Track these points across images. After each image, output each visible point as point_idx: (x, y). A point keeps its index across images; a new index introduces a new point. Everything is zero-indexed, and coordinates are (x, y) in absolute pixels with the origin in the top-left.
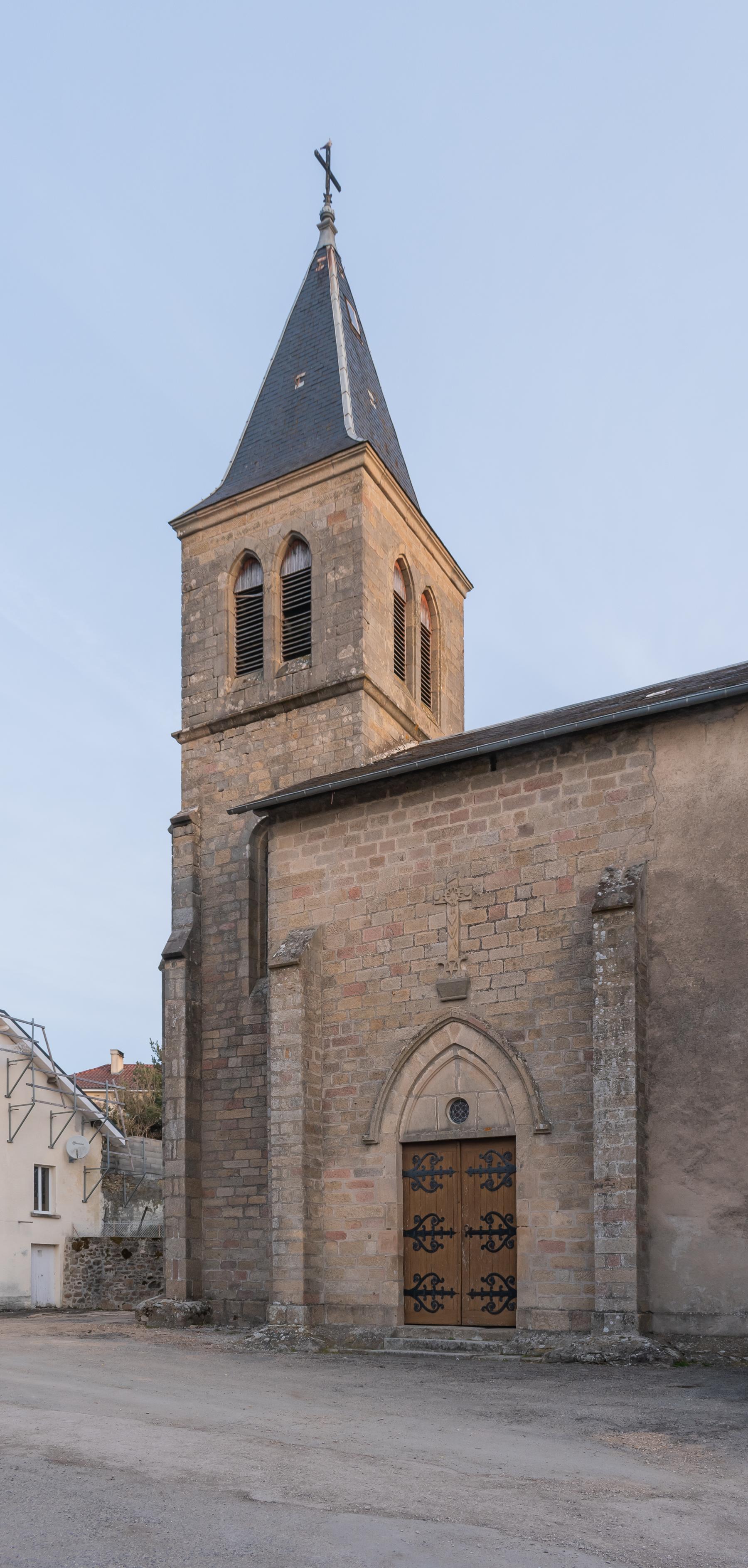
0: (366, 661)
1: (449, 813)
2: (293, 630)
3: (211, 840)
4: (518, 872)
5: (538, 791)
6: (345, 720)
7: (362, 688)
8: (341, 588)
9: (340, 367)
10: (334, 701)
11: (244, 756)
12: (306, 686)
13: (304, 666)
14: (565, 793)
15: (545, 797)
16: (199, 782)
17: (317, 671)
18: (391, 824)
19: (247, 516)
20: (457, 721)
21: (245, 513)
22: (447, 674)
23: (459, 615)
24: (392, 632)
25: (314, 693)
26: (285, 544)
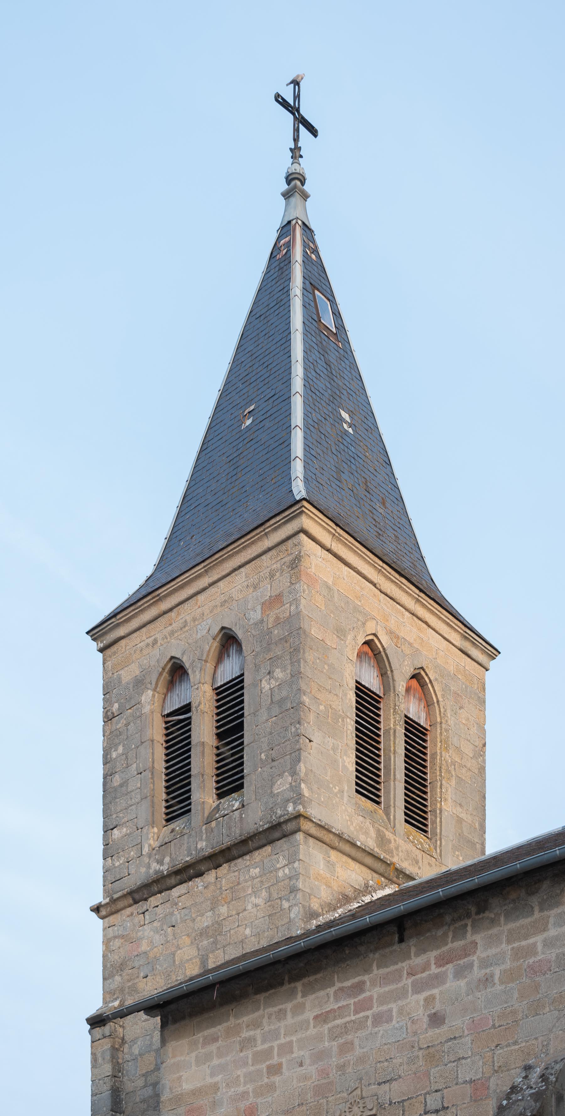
0: (306, 793)
1: (352, 1001)
2: (233, 755)
3: (134, 1041)
4: (427, 1074)
5: (450, 966)
6: (280, 874)
7: (299, 830)
8: (276, 698)
9: (293, 392)
10: (268, 849)
11: (170, 930)
12: (238, 831)
13: (237, 805)
14: (480, 967)
15: (459, 974)
16: (121, 967)
17: (250, 812)
18: (290, 1020)
19: (173, 614)
20: (472, 844)
21: (171, 610)
22: (453, 782)
24: (353, 745)
25: (244, 842)
26: (216, 644)
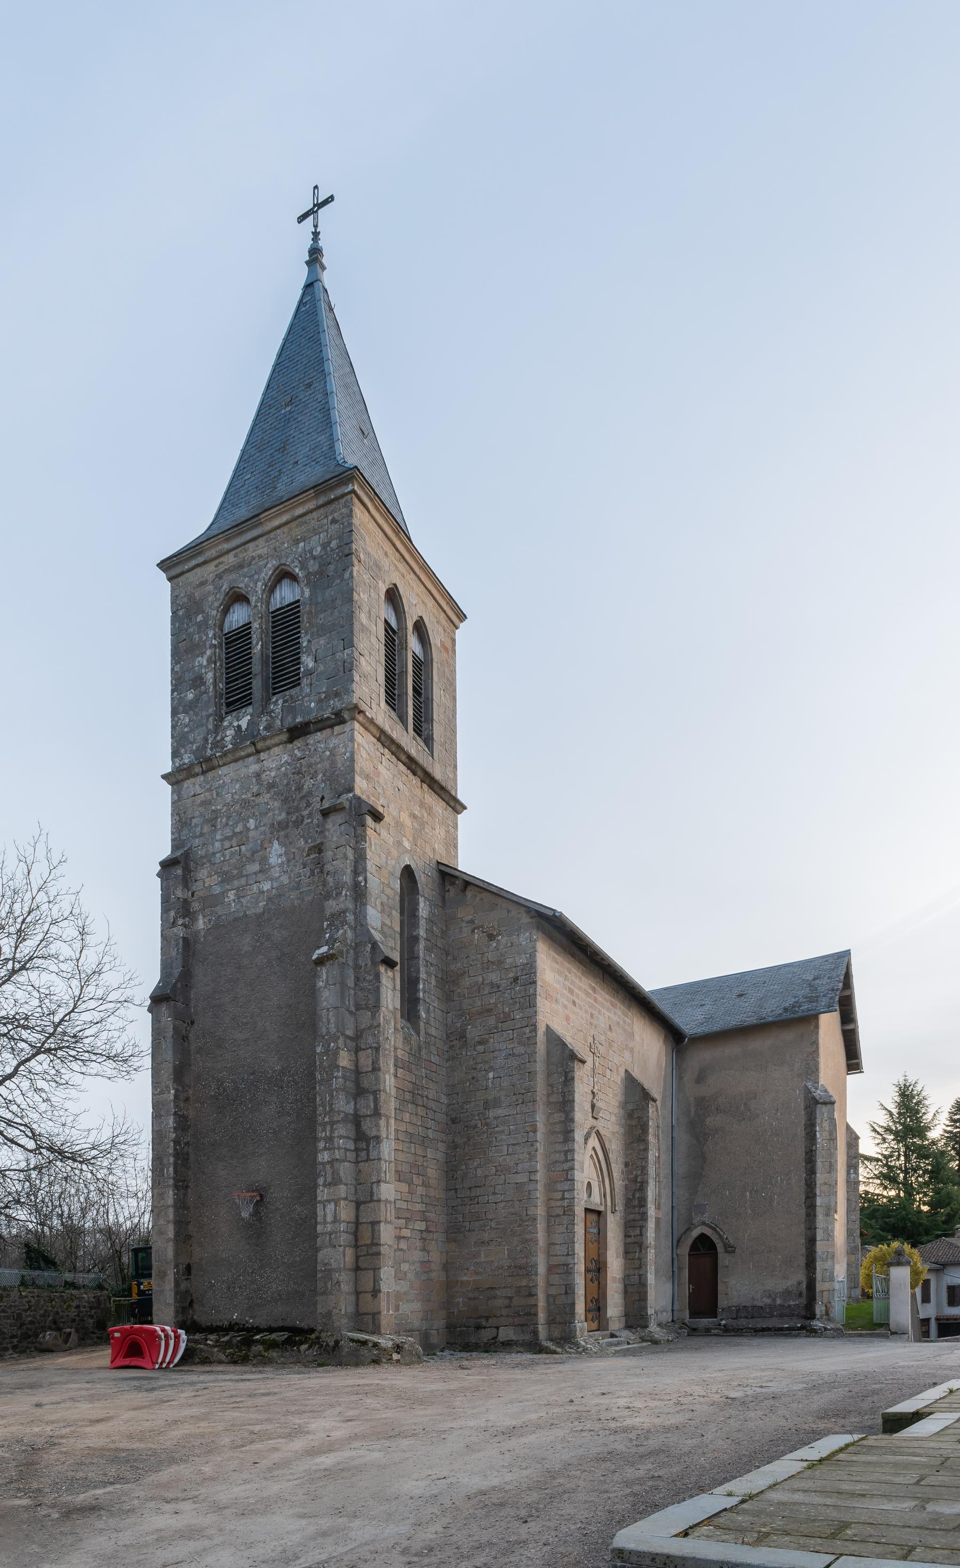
23: (450, 648)
